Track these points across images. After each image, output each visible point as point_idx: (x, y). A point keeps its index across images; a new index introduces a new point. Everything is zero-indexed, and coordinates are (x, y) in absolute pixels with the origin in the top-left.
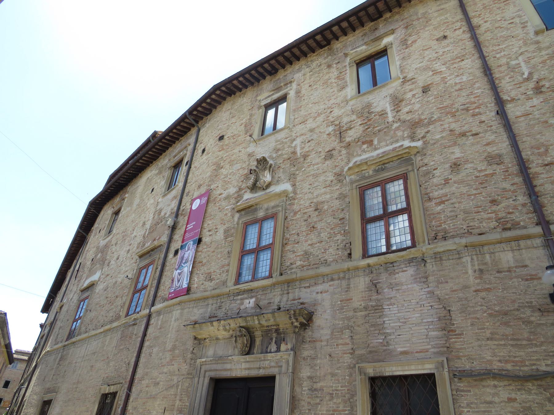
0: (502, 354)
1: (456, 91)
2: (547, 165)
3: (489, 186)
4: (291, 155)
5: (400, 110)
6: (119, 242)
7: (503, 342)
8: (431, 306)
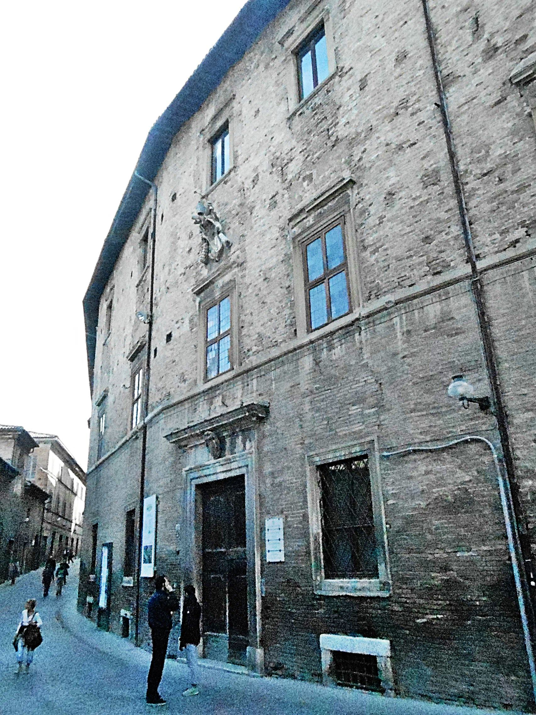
0: (422, 426)
1: (396, 78)
2: (485, 175)
3: (423, 218)
4: (239, 209)
5: (338, 123)
6: (116, 344)
7: (424, 413)
8: (365, 381)
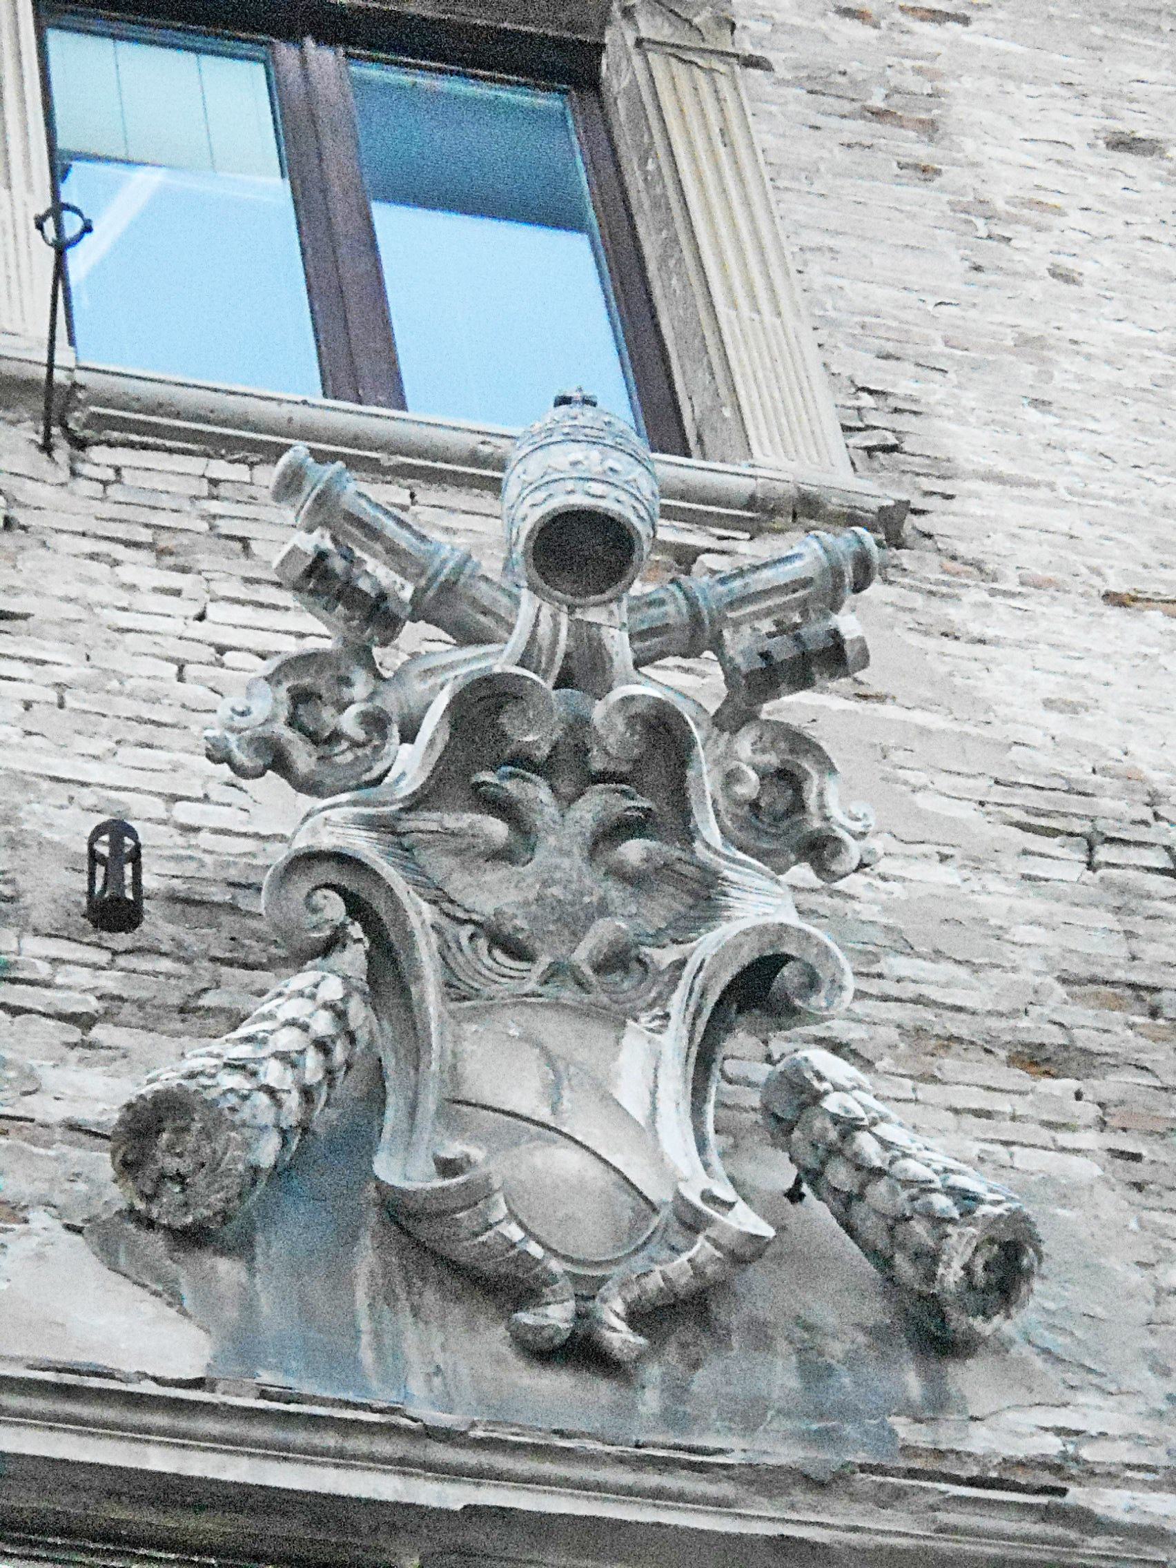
4: (1089, 1025)
